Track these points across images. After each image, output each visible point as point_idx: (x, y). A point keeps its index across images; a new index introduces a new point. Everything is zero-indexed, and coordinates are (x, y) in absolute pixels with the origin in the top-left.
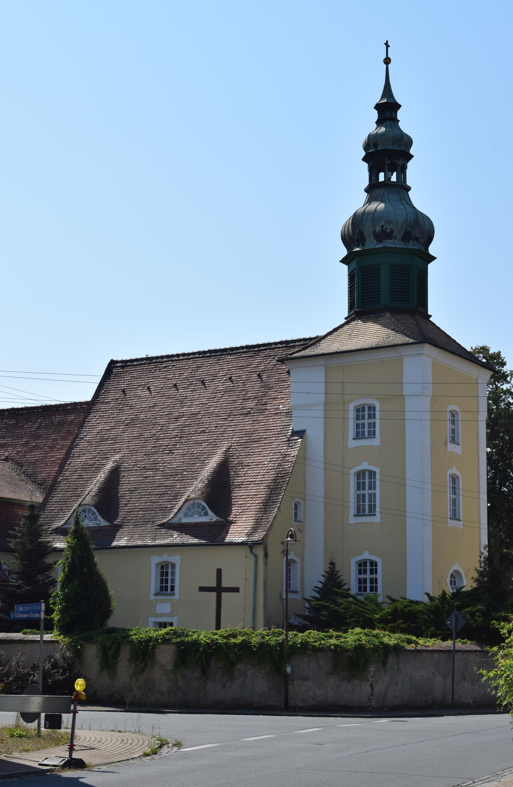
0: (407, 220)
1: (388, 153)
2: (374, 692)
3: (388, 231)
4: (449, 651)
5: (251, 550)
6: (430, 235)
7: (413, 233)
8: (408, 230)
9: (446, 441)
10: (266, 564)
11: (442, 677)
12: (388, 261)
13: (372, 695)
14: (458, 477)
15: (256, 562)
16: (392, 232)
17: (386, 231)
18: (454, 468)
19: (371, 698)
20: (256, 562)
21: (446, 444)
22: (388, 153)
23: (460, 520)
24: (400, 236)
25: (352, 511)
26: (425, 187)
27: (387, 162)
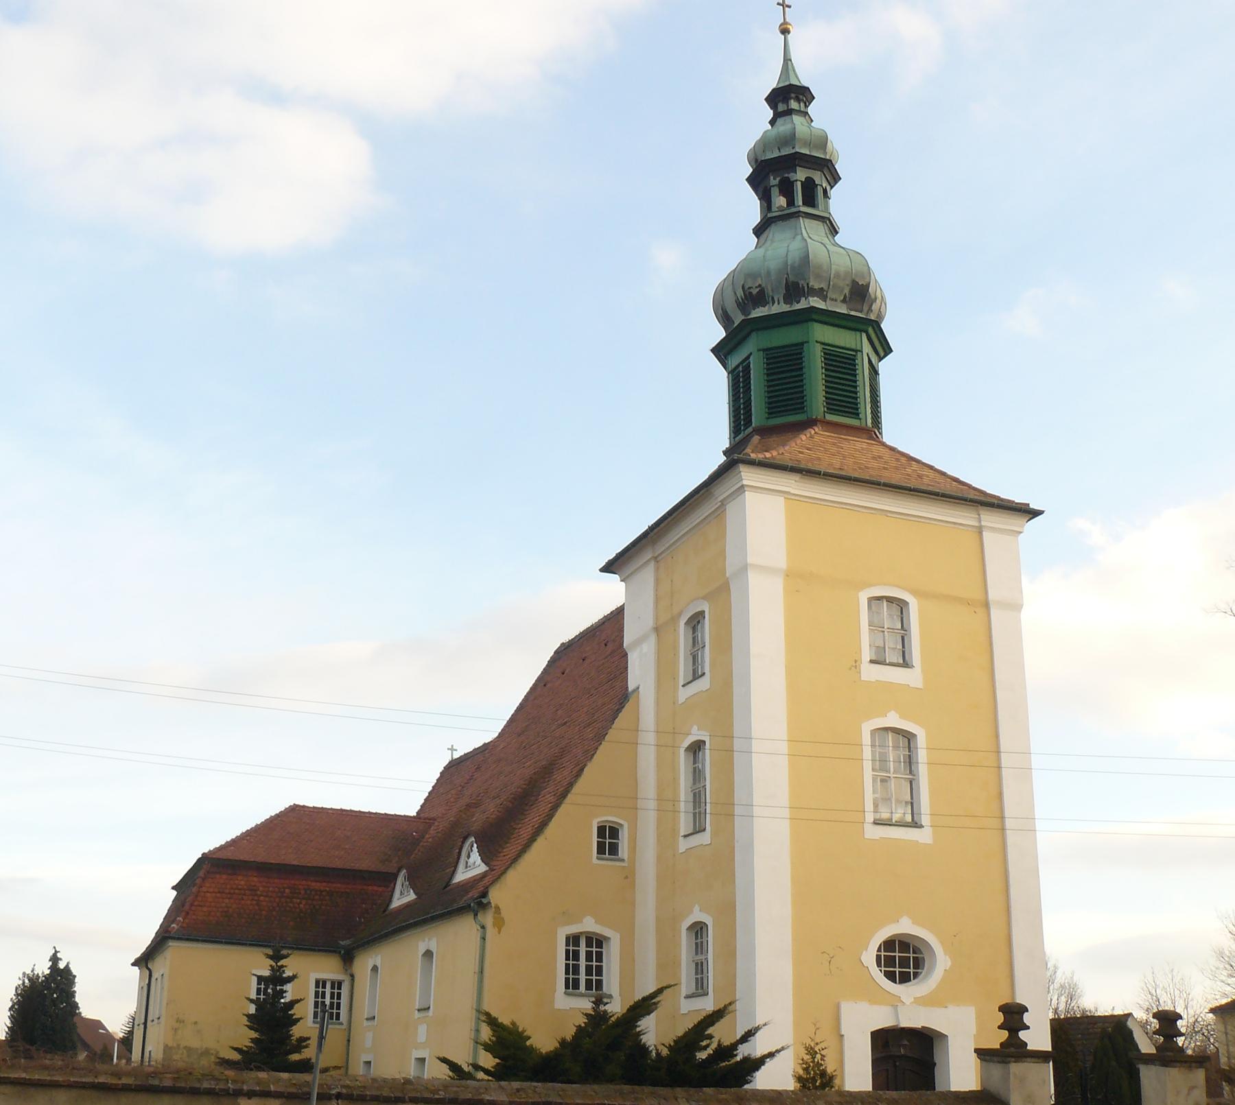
0: (786, 263)
1: (790, 176)
3: (754, 292)
7: (801, 282)
22: (790, 176)
24: (779, 296)
27: (773, 181)
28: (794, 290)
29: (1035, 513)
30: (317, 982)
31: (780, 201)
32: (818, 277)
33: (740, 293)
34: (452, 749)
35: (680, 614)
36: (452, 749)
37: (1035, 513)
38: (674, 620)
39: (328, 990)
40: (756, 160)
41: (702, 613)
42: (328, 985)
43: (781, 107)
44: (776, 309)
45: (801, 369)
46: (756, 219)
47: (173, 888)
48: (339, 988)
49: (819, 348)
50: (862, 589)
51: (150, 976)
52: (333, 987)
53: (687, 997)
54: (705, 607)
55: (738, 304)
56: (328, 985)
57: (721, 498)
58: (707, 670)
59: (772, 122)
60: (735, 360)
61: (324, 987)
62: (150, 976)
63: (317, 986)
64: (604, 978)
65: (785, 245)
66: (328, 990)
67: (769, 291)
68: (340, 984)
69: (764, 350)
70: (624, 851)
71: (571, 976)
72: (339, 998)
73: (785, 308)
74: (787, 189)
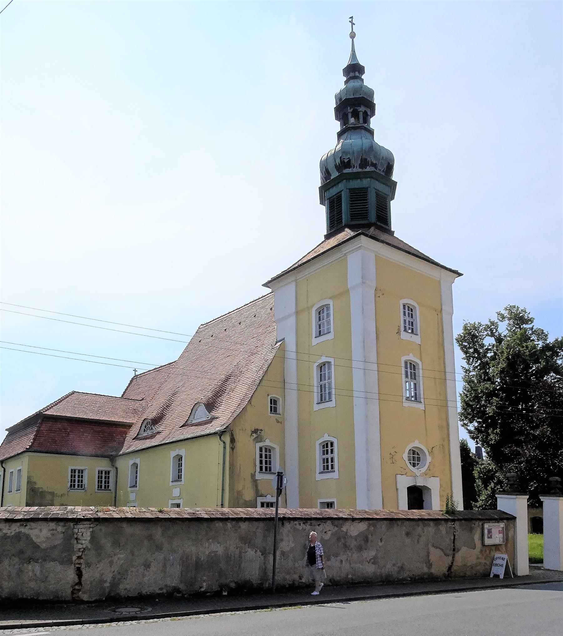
0: (362, 148)
1: (355, 108)
2: (83, 579)
3: (346, 161)
4: (271, 519)
5: (220, 437)
6: (389, 163)
7: (368, 159)
8: (364, 157)
9: (399, 329)
10: (232, 449)
11: (259, 553)
12: (358, 193)
13: (79, 583)
14: (418, 364)
15: (225, 448)
16: (349, 161)
17: (344, 161)
18: (411, 354)
19: (77, 587)
20: (225, 448)
21: (398, 332)
22: (355, 108)
23: (421, 402)
24: (357, 165)
25: (316, 397)
26: (385, 130)
27: (350, 110)
28: (364, 163)
29: (460, 275)
30: (72, 470)
31: (352, 120)
32: (375, 157)
33: (338, 161)
34: (135, 371)
35: (313, 306)
36: (135, 371)
37: (460, 275)
38: (309, 309)
39: (77, 474)
40: (340, 99)
41: (327, 306)
42: (77, 472)
43: (352, 74)
44: (355, 170)
45: (366, 200)
46: (339, 129)
47: (6, 430)
48: (109, 474)
49: (374, 191)
50: (401, 299)
51: (4, 471)
52: (79, 473)
53: (320, 473)
54: (331, 302)
55: (336, 166)
56: (77, 472)
57: (344, 252)
58: (332, 330)
59: (346, 82)
60: (334, 191)
61: (75, 473)
62: (4, 471)
63: (72, 472)
64: (272, 466)
65: (355, 141)
66: (77, 474)
67: (353, 162)
68: (109, 472)
69: (349, 189)
70: (280, 410)
71: (268, 466)
72: (72, 475)
73: (360, 170)
74: (355, 115)
